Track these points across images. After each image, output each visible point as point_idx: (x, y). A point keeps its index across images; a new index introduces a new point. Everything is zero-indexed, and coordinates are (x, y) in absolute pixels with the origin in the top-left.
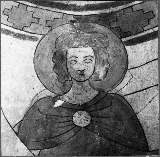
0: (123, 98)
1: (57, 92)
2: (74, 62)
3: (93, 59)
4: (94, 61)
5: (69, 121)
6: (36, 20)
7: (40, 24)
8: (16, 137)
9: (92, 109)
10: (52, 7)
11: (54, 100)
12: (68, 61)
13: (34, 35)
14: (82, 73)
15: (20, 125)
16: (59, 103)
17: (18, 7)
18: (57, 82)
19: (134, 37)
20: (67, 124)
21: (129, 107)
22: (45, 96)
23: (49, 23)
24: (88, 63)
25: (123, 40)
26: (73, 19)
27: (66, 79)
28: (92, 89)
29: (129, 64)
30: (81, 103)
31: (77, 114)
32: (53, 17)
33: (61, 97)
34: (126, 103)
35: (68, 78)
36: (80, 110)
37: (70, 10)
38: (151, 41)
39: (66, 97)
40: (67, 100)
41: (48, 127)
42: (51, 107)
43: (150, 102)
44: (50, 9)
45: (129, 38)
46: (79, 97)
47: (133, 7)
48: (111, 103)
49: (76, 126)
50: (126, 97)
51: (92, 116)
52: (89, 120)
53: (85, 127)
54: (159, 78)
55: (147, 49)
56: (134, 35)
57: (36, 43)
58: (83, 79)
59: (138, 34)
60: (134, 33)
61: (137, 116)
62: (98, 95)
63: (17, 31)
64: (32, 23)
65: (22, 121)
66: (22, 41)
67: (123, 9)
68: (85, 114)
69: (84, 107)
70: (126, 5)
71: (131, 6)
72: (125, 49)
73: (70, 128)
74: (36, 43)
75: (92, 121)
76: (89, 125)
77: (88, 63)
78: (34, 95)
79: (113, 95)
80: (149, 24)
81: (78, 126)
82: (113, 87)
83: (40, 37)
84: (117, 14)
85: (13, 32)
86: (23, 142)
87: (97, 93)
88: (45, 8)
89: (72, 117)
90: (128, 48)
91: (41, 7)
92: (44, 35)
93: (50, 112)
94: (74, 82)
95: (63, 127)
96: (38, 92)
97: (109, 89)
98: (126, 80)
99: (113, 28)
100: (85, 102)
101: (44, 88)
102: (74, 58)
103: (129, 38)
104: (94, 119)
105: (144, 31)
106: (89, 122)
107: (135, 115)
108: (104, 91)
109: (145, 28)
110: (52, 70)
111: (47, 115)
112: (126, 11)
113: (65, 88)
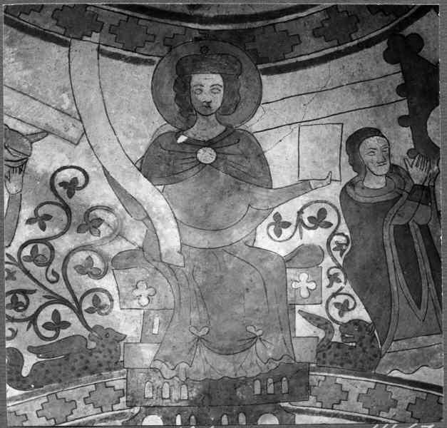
0: (252, 135)
1: (180, 126)
2: (198, 92)
3: (222, 89)
4: (222, 92)
5: (193, 158)
6: (151, 38)
7: (156, 42)
8: (139, 173)
9: (218, 145)
10: (172, 20)
11: (177, 135)
12: (191, 89)
13: (150, 57)
14: (208, 105)
15: (142, 161)
16: (182, 139)
17: (127, 21)
18: (180, 116)
19: (272, 65)
20: (191, 160)
21: (257, 145)
22: (166, 131)
23: (168, 41)
24: (215, 93)
25: (260, 67)
26: (198, 35)
27: (190, 113)
28: (219, 124)
29: (263, 98)
30: (206, 139)
31: (201, 151)
32: (172, 33)
33: (185, 132)
34: (254, 140)
35: (192, 111)
36: (205, 147)
37: (195, 23)
38: (291, 73)
39: (191, 133)
40: (191, 135)
41: (171, 163)
42: (174, 143)
43: (280, 141)
44: (169, 21)
45: (267, 65)
46: (204, 133)
47: (277, 26)
48: (239, 140)
49: (200, 162)
50: (255, 134)
51: (217, 153)
52: (214, 157)
53: (210, 164)
54: (430, 114)
55: (285, 82)
56: (274, 62)
57: (153, 68)
58: (209, 112)
59: (279, 61)
60: (273, 60)
61: (265, 154)
62: (225, 131)
63: (128, 54)
64: (146, 41)
65: (143, 157)
66: (136, 66)
67: (263, 26)
68: (209, 150)
69: (209, 144)
70: (162, 219)
71: (274, 25)
72: (261, 79)
73: (193, 164)
74: (153, 68)
75: (217, 158)
76: (214, 162)
77: (215, 93)
78: (154, 129)
79: (241, 132)
80: (292, 51)
81: (203, 163)
82: (242, 122)
83: (157, 59)
84: (256, 32)
85: (124, 56)
86: (146, 178)
87: (224, 128)
88: (162, 21)
89: (196, 153)
90: (264, 78)
91: (156, 19)
92: (163, 57)
93: (172, 147)
94: (199, 116)
95: (187, 163)
96: (158, 126)
97: (237, 125)
98: (257, 116)
99: (248, 50)
100: (211, 138)
101: (166, 122)
102: (199, 87)
103: (267, 65)
104: (219, 156)
105: (284, 59)
106: (214, 159)
107: (263, 153)
108: (232, 127)
109: (287, 56)
110: (173, 102)
111: (169, 151)
112: (266, 29)
113: (189, 124)
